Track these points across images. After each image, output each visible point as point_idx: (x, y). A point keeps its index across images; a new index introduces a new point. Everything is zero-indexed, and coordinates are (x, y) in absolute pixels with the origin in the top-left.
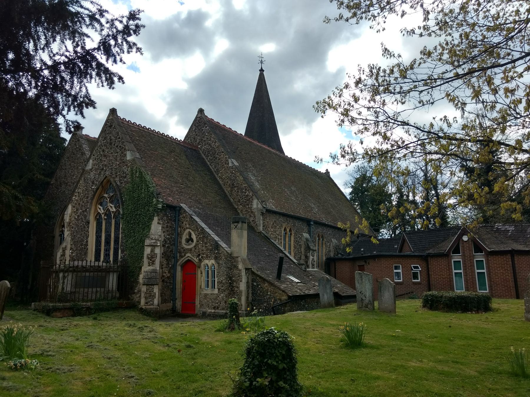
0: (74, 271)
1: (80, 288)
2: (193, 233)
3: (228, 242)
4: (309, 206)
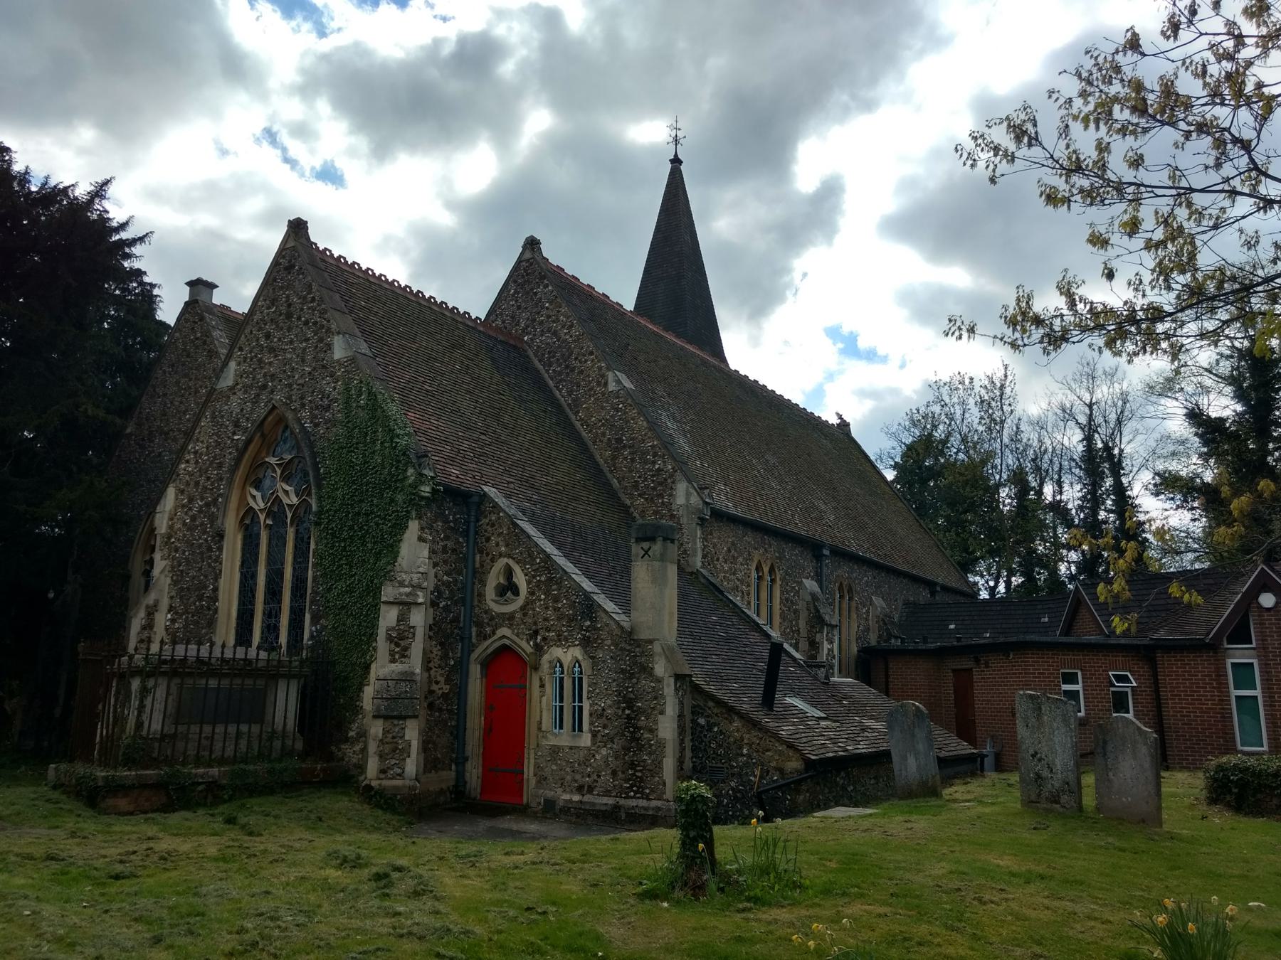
0: (173, 674)
2: (517, 569)
3: (624, 599)
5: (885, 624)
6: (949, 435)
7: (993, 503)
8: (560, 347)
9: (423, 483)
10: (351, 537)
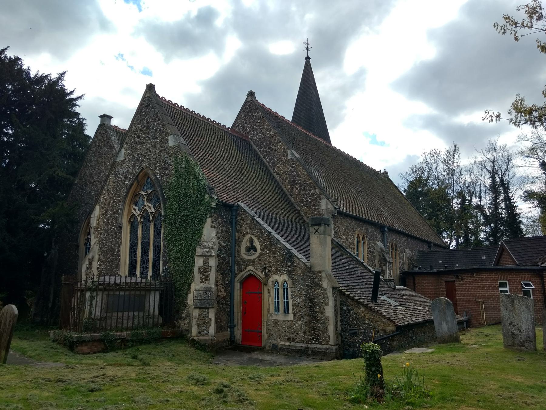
0: (105, 289)
1: (112, 312)
2: (255, 239)
4: (379, 210)
6: (429, 177)
7: (450, 207)
8: (265, 140)
9: (212, 201)
10: (180, 226)
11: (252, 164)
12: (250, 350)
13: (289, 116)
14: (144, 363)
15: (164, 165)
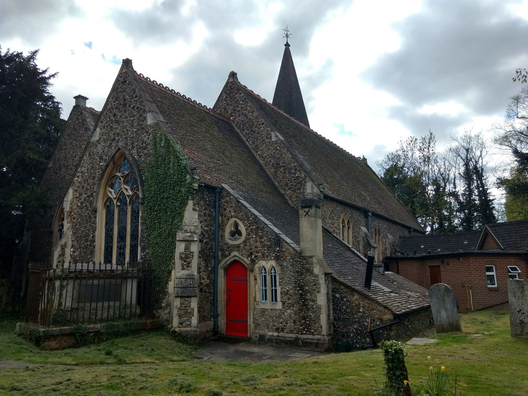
0: (77, 278)
1: (85, 302)
2: (240, 223)
5: (393, 246)
6: (404, 164)
8: (248, 121)
10: (159, 210)
11: (234, 146)
12: (235, 341)
13: (270, 100)
14: (120, 360)
15: (142, 144)
